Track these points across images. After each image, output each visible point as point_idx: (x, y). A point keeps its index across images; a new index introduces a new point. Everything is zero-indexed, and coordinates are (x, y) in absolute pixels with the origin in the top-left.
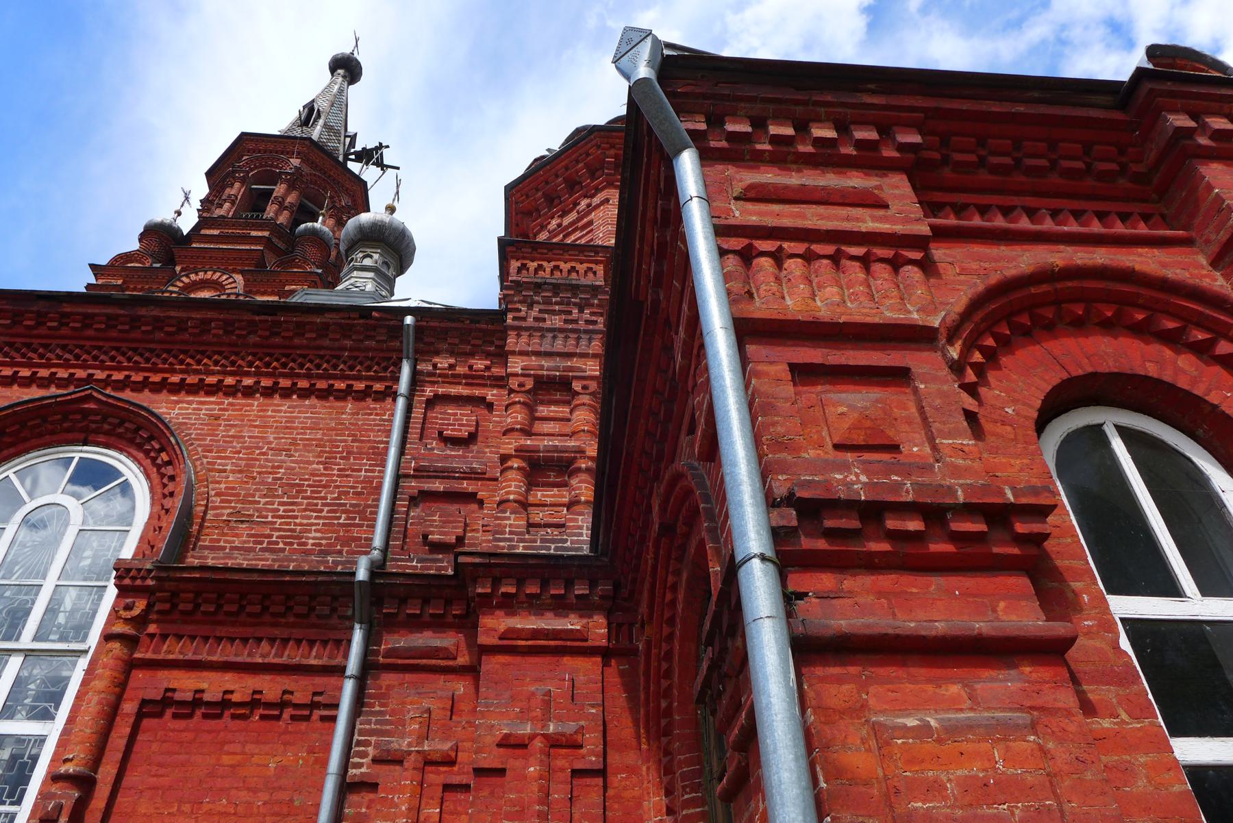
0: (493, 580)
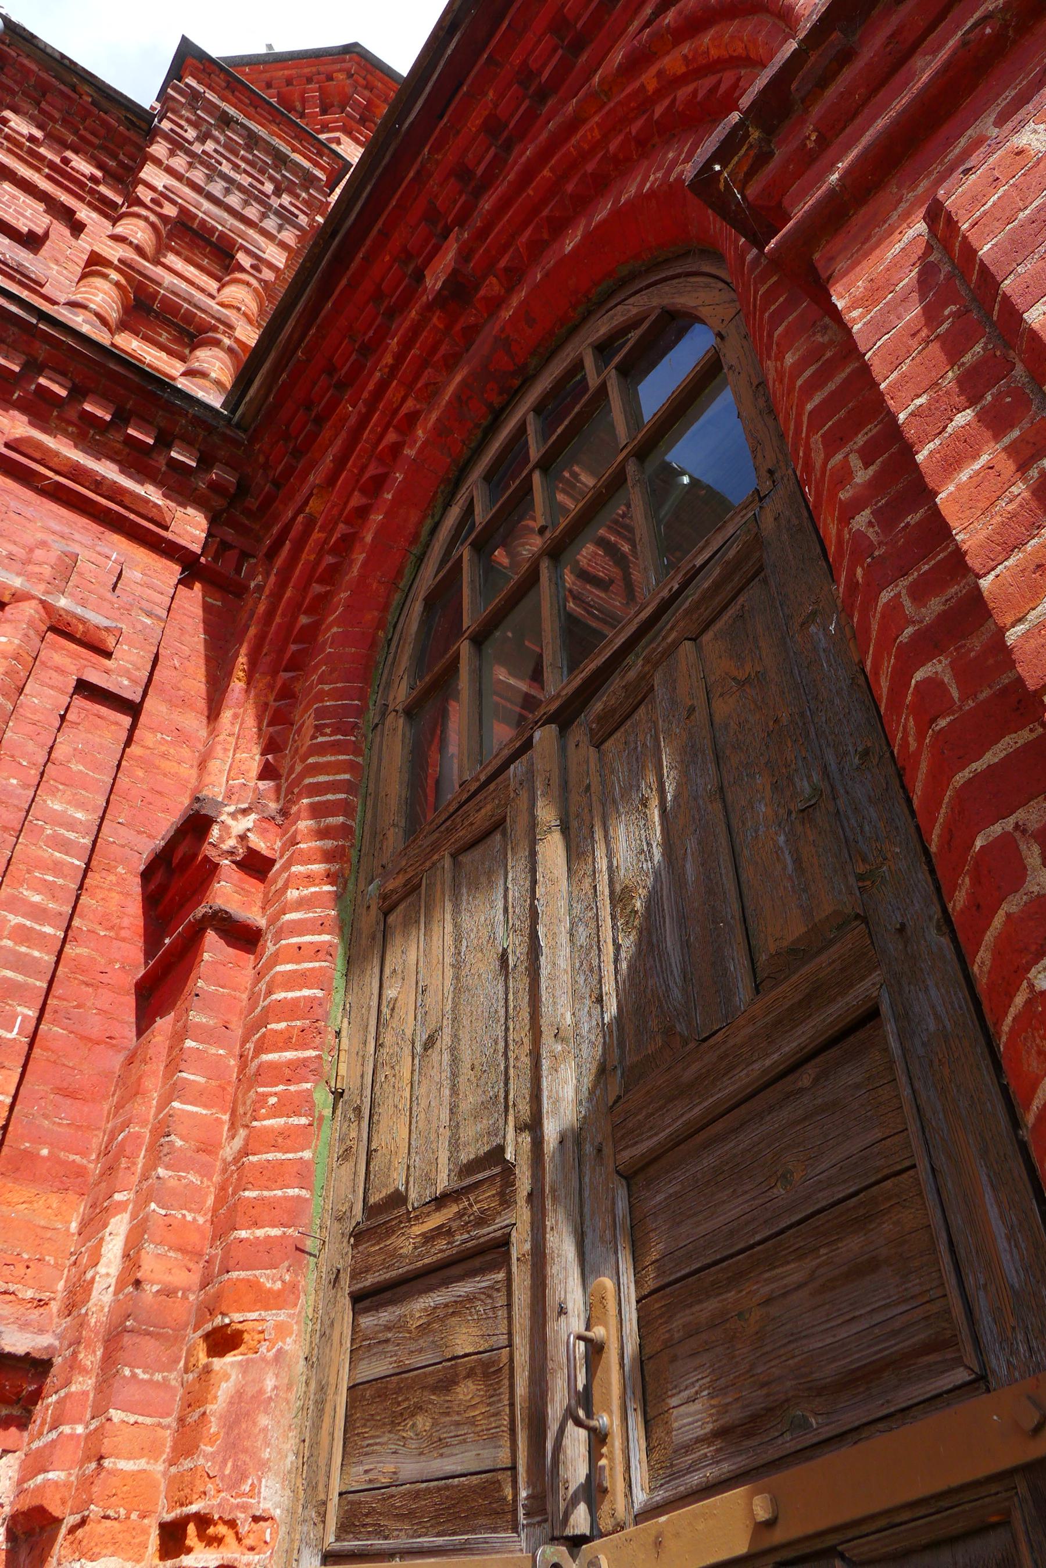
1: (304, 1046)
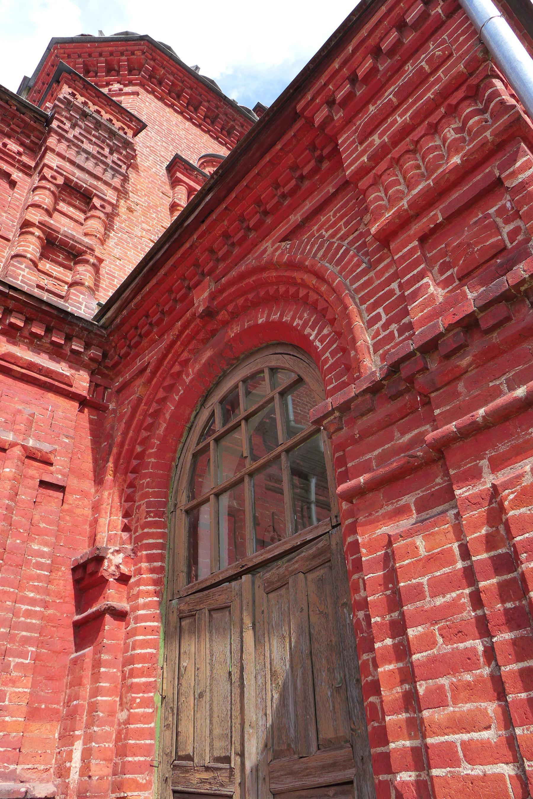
0: (5, 309)
1: (149, 676)
